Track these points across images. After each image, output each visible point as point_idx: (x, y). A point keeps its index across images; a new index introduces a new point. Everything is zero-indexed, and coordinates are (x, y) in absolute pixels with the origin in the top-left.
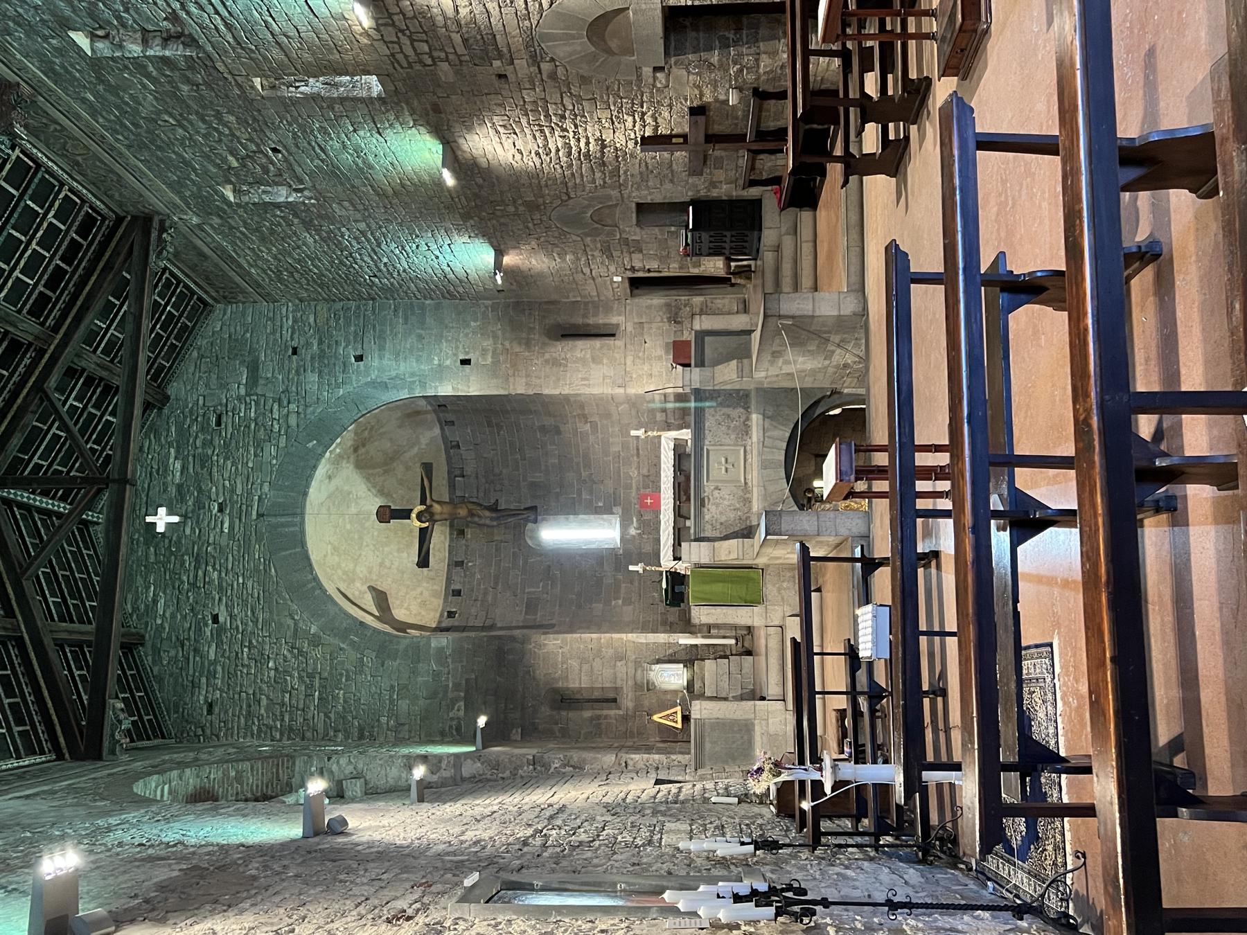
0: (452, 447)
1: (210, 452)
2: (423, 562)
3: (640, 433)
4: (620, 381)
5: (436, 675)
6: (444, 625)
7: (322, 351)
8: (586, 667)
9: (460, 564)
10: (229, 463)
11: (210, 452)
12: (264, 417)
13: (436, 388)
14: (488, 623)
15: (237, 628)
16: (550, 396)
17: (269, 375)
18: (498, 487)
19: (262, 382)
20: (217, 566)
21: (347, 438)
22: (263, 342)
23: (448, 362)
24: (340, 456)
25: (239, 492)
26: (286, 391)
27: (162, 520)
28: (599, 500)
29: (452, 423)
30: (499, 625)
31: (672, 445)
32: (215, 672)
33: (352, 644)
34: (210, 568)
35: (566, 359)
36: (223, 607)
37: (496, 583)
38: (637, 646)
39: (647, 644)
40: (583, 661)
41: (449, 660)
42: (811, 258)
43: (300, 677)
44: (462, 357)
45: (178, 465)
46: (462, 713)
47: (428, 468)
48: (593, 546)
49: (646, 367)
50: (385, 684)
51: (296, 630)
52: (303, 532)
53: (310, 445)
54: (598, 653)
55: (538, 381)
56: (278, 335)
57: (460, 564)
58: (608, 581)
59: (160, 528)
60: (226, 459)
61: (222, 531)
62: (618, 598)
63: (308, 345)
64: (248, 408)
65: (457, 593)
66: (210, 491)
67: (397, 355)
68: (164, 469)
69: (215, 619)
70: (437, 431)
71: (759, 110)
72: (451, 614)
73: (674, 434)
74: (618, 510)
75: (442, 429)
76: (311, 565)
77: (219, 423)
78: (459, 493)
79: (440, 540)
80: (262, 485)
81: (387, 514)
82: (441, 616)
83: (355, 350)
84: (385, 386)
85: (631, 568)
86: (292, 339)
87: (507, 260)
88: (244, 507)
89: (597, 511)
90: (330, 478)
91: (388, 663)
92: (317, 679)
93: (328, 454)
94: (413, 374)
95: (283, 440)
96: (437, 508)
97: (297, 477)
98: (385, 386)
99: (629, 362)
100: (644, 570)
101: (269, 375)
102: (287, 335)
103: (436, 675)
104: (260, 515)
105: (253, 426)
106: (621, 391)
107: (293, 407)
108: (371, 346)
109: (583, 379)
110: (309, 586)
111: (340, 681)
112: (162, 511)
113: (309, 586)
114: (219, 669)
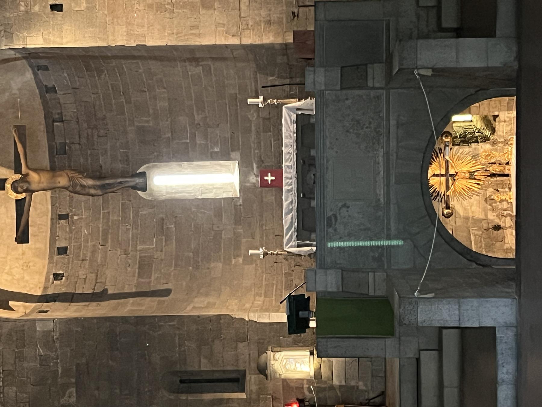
0: (47, 90)
2: (23, 237)
5: (44, 360)
6: (50, 292)
13: (24, 39)
18: (102, 132)
28: (216, 144)
29: (46, 68)
30: (110, 292)
31: (294, 117)
37: (105, 240)
41: (57, 345)
42: (424, 392)
46: (73, 400)
48: (210, 196)
55: (140, 31)
57: (62, 217)
58: (226, 235)
62: (238, 256)
65: (62, 251)
70: (29, 75)
73: (295, 104)
74: (236, 155)
75: (35, 74)
78: (59, 140)
89: (214, 157)
96: (34, 176)
109: (193, 27)
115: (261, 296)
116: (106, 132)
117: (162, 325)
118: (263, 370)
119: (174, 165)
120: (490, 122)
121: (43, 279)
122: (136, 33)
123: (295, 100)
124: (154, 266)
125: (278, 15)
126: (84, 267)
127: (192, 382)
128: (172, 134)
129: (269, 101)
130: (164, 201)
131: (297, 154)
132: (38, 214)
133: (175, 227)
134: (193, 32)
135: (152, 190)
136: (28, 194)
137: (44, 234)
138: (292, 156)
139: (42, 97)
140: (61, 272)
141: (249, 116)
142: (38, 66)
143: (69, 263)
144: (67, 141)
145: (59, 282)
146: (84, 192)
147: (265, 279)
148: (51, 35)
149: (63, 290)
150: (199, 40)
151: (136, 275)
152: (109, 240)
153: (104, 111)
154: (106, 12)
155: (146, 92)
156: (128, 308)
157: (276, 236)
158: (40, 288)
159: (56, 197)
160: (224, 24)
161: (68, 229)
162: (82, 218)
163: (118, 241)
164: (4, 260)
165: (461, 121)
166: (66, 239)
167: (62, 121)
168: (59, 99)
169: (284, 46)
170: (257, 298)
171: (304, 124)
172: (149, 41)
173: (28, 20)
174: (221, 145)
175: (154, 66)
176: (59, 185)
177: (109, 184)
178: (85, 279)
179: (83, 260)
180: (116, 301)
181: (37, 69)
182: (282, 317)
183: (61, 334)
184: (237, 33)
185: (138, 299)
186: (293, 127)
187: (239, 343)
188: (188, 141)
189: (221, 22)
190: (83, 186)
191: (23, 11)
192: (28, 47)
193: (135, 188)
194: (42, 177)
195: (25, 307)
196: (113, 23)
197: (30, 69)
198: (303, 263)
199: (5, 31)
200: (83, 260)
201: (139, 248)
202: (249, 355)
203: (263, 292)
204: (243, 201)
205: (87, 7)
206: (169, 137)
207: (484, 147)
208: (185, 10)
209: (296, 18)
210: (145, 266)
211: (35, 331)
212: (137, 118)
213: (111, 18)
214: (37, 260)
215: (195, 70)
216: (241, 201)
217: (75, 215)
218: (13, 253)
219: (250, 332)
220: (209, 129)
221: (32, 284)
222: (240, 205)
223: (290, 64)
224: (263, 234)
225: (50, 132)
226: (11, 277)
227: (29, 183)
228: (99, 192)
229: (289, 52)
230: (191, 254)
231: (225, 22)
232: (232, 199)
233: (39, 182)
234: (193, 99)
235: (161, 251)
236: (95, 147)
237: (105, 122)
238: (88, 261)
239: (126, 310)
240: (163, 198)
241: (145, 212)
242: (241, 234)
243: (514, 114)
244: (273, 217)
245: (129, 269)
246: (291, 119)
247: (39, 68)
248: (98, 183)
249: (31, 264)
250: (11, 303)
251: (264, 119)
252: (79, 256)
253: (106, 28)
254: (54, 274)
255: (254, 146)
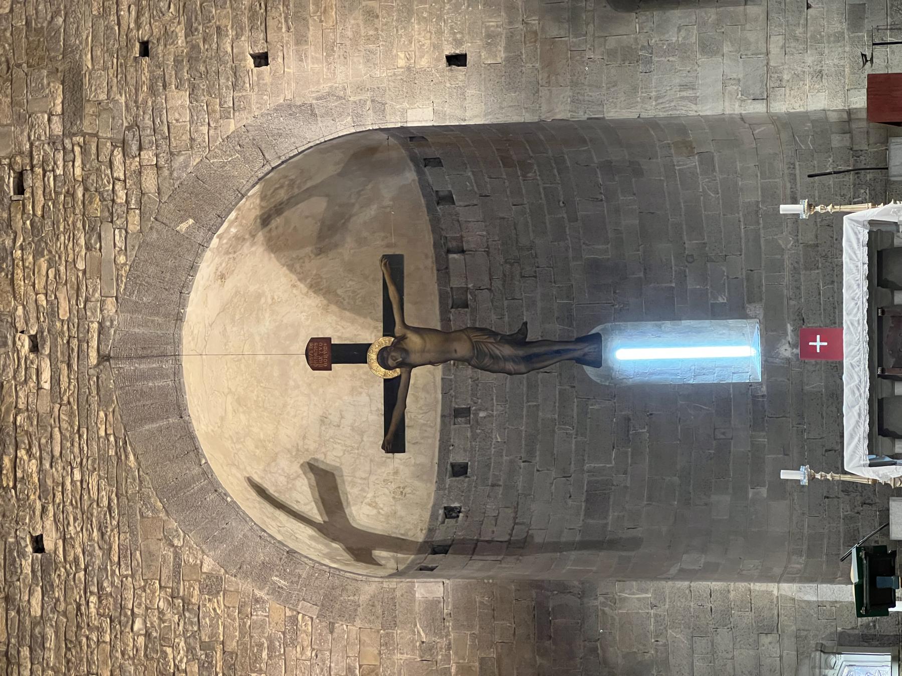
1: (8, 243)
2: (394, 441)
3: (799, 208)
4: (756, 90)
7: (194, 47)
8: (701, 645)
9: (461, 413)
10: (43, 263)
11: (8, 243)
12: (99, 176)
13: (404, 112)
14: (519, 533)
15: (76, 560)
16: (622, 125)
17: (103, 97)
19: (89, 109)
20: (35, 450)
21: (251, 205)
22: (86, 33)
23: (424, 63)
24: (239, 239)
25: (64, 314)
26: (134, 125)
30: (538, 539)
31: (864, 236)
32: (44, 637)
33: (276, 591)
34: (22, 453)
35: (649, 47)
36: (49, 522)
37: (531, 452)
38: (801, 608)
39: (820, 605)
40: (696, 632)
43: (190, 649)
44: (450, 50)
47: (394, 266)
48: (710, 379)
49: (810, 58)
51: (177, 566)
52: (179, 389)
53: (183, 227)
54: (724, 617)
56: (113, 18)
57: (461, 413)
60: (38, 254)
61: (39, 388)
63: (168, 36)
64: (69, 160)
65: (460, 470)
66: (13, 314)
67: (329, 49)
69: (38, 544)
70: (410, 176)
72: (450, 513)
73: (867, 212)
74: (757, 309)
75: (420, 173)
76: (196, 449)
77: (20, 190)
78: (456, 282)
79: (425, 385)
80: (103, 303)
81: (325, 354)
82: (434, 516)
83: (255, 43)
84: (310, 112)
85: (785, 475)
86: (138, 26)
88: (75, 343)
89: (716, 313)
90: (222, 277)
91: (341, 627)
92: (219, 654)
93: (215, 241)
94: (360, 88)
95: (134, 219)
97: (162, 285)
98: (310, 112)
99: (775, 49)
100: (812, 479)
101: (103, 97)
102: (128, 18)
103: (428, 649)
104: (104, 358)
105: (80, 193)
106: (759, 108)
107: (148, 156)
108: (281, 38)
109: (684, 87)
110: (196, 487)
111: (257, 658)
113: (196, 487)
114: (50, 632)
115: (801, 556)
116: (534, 269)
117: (625, 598)
119: (649, 325)
121: (427, 516)
122: (587, 98)
123: (866, 205)
124: (612, 497)
125: (836, 61)
126: (496, 497)
128: (645, 273)
129: (818, 208)
130: (630, 388)
131: (868, 300)
132: (420, 408)
133: (648, 431)
134: (684, 94)
135: (610, 369)
136: (404, 369)
137: (430, 441)
138: (860, 303)
139: (430, 210)
140: (456, 505)
141: (780, 242)
142: (425, 159)
143: (469, 491)
144: (470, 286)
145: (453, 521)
146: (496, 367)
147: (808, 526)
148: (447, 105)
149: (460, 534)
150: (694, 107)
151: (582, 513)
152: (538, 453)
153: (531, 234)
154: (537, 65)
155: (602, 200)
157: (826, 451)
158: (422, 530)
159: (451, 380)
160: (739, 80)
161: (469, 434)
162: (492, 416)
163: (553, 454)
164: (366, 482)
166: (465, 451)
167: (463, 251)
168: (457, 214)
169: (845, 116)
170: (794, 557)
172: (608, 112)
174: (729, 294)
176: (455, 356)
177: (537, 355)
178: (496, 518)
179: (493, 485)
180: (548, 555)
183: (454, 607)
184: (762, 93)
185: (586, 553)
186: (862, 254)
187: (763, 636)
188: (673, 285)
189: (734, 76)
190: (494, 357)
191: (401, 68)
192: (409, 125)
193: (581, 361)
194: (427, 339)
195: (397, 561)
196: (549, 82)
197: (411, 165)
198: (877, 500)
199: (373, 101)
200: (493, 485)
201: (586, 467)
202: (781, 657)
203: (805, 547)
204: (767, 387)
205: (506, 57)
206: (640, 278)
208: (671, 59)
209: (869, 63)
210: (596, 498)
211: (413, 599)
212: (587, 245)
213: (546, 75)
214: (417, 483)
216: (764, 389)
217: (480, 410)
218: (379, 471)
219: (782, 618)
220: (709, 265)
221: (409, 523)
222: (763, 396)
223: (856, 148)
224: (803, 447)
225: (443, 271)
226: (375, 512)
227: (406, 351)
228: (522, 368)
229: (854, 126)
230: (676, 479)
231: (741, 76)
232: (750, 385)
233: (423, 351)
234: (683, 214)
235: (625, 473)
236: (517, 296)
237: (533, 251)
238: (501, 489)
239: (564, 571)
240: (630, 382)
241: (596, 407)
242: (765, 446)
244: (823, 418)
245: (570, 502)
246: (858, 239)
247: (428, 162)
248: (521, 352)
249: (408, 490)
250: (378, 553)
251: (807, 246)
252: (487, 479)
253: (537, 92)
254: (445, 508)
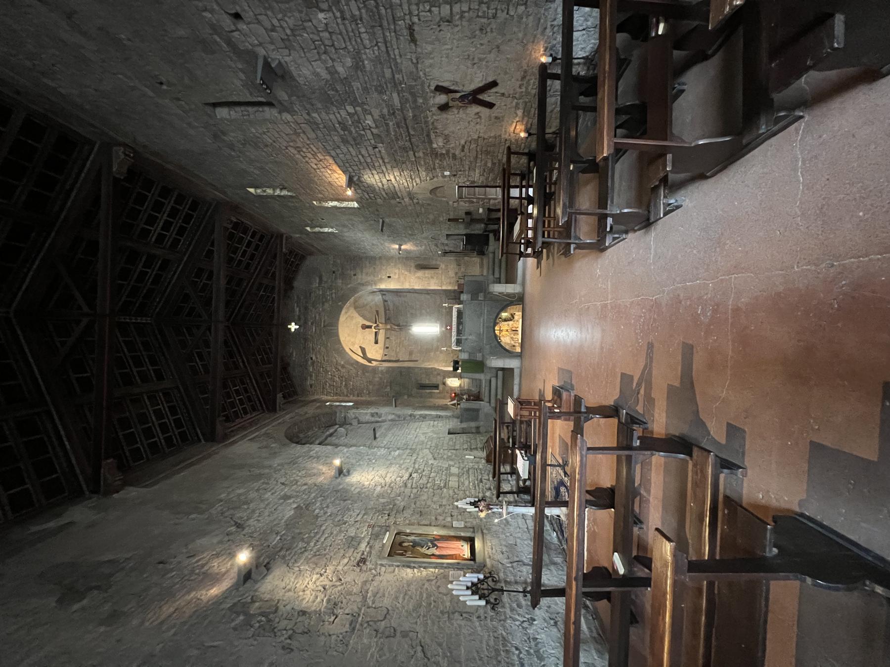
0: (385, 301)
2: (376, 342)
5: (381, 378)
27: (293, 327)
45: (298, 309)
50: (365, 380)
59: (293, 330)
68: (293, 311)
71: (489, 215)
81: (365, 327)
87: (403, 247)
103: (381, 378)
108: (358, 270)
112: (293, 324)
118: (444, 384)
120: (513, 316)
127: (423, 387)
128: (394, 77)
156: (406, 364)
165: (504, 315)
171: (460, 314)
173: (381, 280)
175: (416, 295)
181: (383, 295)
182: (451, 369)
207: (511, 323)
210: (411, 353)
215: (428, 297)
243: (631, 639)
255: (444, 317)
